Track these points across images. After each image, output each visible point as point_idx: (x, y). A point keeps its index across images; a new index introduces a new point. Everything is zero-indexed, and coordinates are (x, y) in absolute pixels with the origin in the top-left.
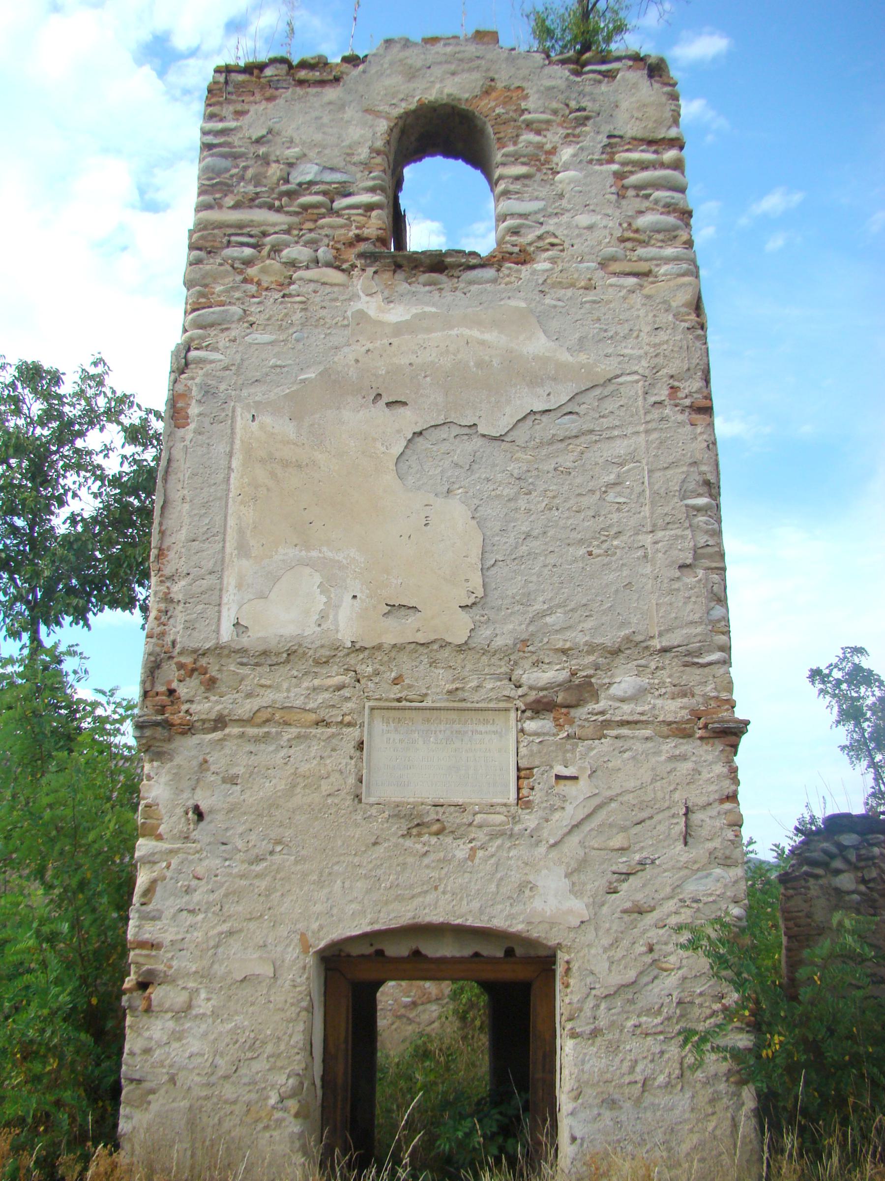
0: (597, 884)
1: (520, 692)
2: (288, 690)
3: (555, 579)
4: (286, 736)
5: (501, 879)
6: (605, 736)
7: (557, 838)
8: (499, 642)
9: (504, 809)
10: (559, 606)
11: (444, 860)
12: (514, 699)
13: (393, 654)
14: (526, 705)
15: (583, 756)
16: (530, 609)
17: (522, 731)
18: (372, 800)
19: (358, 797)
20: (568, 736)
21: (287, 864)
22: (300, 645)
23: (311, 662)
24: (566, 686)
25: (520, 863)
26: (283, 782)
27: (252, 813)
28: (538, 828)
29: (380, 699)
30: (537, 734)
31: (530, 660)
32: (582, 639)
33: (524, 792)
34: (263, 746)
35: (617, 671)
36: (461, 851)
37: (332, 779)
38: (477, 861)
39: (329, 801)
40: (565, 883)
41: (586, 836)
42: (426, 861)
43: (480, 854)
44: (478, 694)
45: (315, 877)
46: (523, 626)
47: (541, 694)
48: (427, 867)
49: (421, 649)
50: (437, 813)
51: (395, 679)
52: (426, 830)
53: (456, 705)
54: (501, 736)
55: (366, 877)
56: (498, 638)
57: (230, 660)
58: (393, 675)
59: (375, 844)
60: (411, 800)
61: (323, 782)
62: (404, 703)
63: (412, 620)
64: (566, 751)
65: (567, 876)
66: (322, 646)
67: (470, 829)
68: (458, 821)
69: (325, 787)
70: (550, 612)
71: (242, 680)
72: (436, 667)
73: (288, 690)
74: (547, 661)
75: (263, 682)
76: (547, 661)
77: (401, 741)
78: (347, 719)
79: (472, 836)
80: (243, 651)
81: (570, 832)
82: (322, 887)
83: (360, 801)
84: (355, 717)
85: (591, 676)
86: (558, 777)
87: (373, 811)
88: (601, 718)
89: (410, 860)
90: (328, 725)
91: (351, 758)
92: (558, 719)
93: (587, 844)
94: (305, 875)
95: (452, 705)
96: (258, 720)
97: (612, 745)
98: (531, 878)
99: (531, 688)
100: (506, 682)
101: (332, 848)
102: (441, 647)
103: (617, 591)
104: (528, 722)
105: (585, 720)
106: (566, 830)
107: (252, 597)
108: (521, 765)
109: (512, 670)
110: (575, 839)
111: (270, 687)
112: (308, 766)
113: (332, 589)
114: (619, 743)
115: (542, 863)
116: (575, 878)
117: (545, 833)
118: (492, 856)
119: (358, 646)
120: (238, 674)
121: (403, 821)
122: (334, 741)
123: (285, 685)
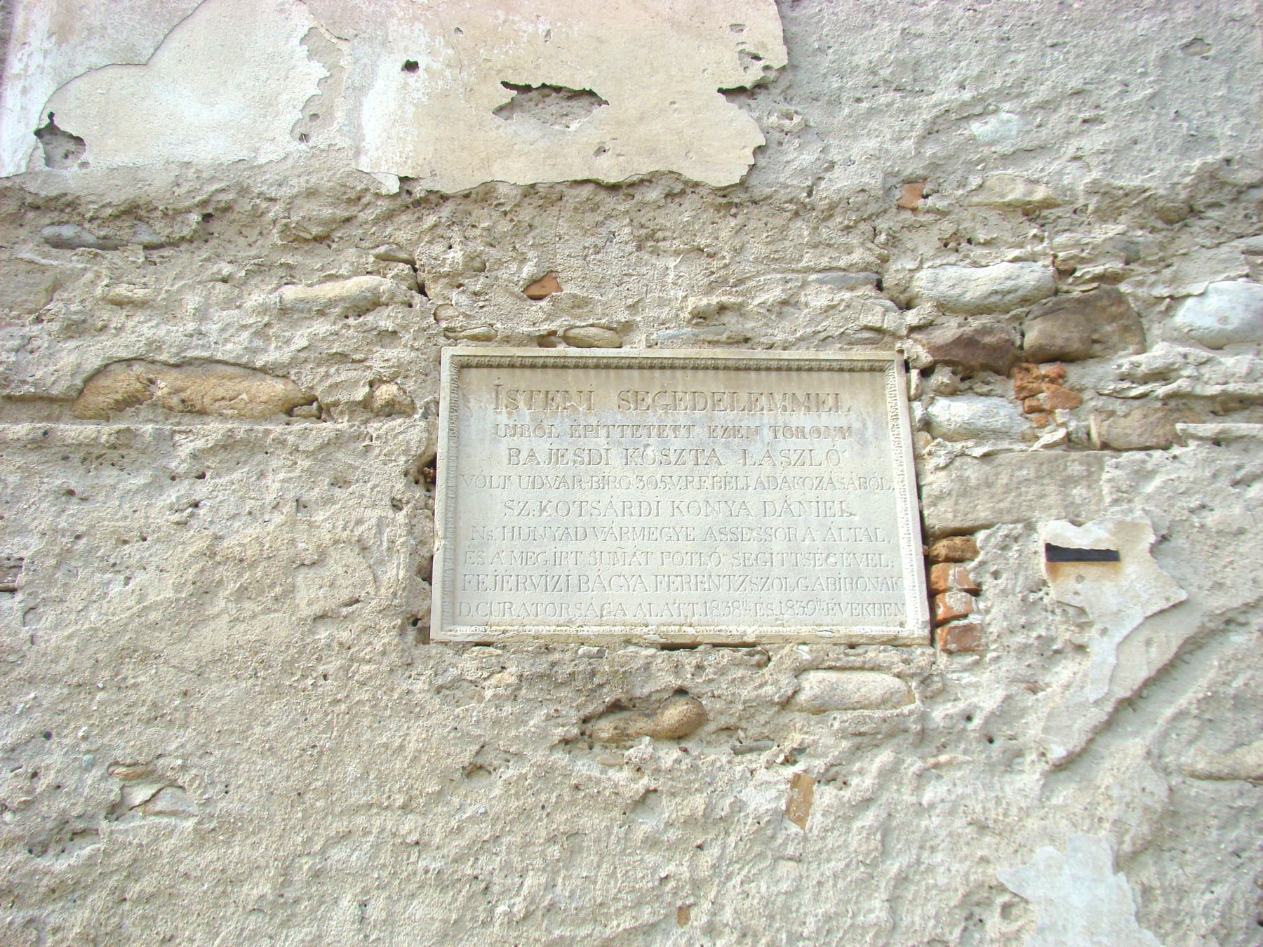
0: (1222, 890)
1: (912, 317)
2: (205, 313)
3: (986, 28)
4: (187, 446)
5: (902, 880)
6: (1181, 440)
7: (1076, 741)
8: (840, 182)
9: (893, 656)
10: (1003, 94)
11: (708, 820)
12: (895, 336)
13: (526, 214)
14: (933, 350)
15: (1123, 496)
16: (923, 101)
17: (927, 425)
18: (463, 632)
19: (417, 624)
20: (1069, 442)
21: (167, 846)
22: (243, 191)
23: (275, 237)
24: (1047, 301)
25: (959, 823)
26: (170, 579)
27: (55, 681)
28: (1006, 712)
29: (487, 338)
30: (973, 433)
31: (935, 234)
32: (1079, 180)
33: (952, 601)
34: (109, 476)
35: (1189, 267)
36: (763, 788)
37: (334, 567)
38: (816, 820)
39: (323, 634)
40: (1116, 891)
41: (1165, 735)
42: (646, 825)
43: (825, 796)
44: (786, 324)
45: (266, 888)
46: (908, 144)
47: (975, 323)
48: (652, 843)
49: (610, 202)
50: (677, 668)
51: (534, 282)
52: (641, 724)
53: (720, 353)
54: (863, 442)
55: (442, 882)
56: (837, 171)
57: (23, 233)
58: (528, 270)
59: (474, 770)
60: (591, 630)
61: (300, 578)
62: (562, 349)
63: (584, 128)
64: (1069, 481)
65: (1124, 863)
66: (311, 193)
67: (786, 718)
68: (746, 692)
69: (310, 593)
70: (981, 108)
71: (56, 286)
72: (655, 252)
73: (202, 314)
74: (981, 236)
75: (122, 290)
76: (981, 236)
77: (556, 456)
78: (385, 392)
79: (795, 739)
80: (65, 205)
81: (1109, 725)
82: (285, 924)
83: (424, 636)
84: (410, 386)
85: (1115, 278)
86: (1056, 554)
87: (469, 665)
88: (1161, 390)
89: (592, 821)
90: (323, 413)
91: (396, 506)
92: (1033, 394)
93: (1169, 759)
94: (229, 881)
95: (707, 352)
96: (99, 399)
97: (1208, 461)
98: (1000, 872)
99: (944, 307)
100: (869, 290)
101: (329, 787)
102: (670, 195)
103: (1164, 59)
104: (942, 402)
105: (1115, 395)
106: (1098, 715)
107: (96, 59)
108: (934, 522)
109: (884, 260)
110: (1129, 748)
111: (142, 304)
112: (254, 530)
113: (344, 47)
114: (1227, 458)
115: (1032, 824)
116: (1148, 874)
117: (1032, 728)
118: (867, 802)
119: (418, 191)
120: (43, 269)
121: (564, 693)
122: (343, 457)
123: (192, 301)
